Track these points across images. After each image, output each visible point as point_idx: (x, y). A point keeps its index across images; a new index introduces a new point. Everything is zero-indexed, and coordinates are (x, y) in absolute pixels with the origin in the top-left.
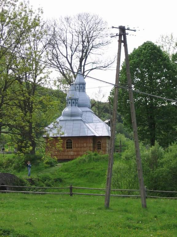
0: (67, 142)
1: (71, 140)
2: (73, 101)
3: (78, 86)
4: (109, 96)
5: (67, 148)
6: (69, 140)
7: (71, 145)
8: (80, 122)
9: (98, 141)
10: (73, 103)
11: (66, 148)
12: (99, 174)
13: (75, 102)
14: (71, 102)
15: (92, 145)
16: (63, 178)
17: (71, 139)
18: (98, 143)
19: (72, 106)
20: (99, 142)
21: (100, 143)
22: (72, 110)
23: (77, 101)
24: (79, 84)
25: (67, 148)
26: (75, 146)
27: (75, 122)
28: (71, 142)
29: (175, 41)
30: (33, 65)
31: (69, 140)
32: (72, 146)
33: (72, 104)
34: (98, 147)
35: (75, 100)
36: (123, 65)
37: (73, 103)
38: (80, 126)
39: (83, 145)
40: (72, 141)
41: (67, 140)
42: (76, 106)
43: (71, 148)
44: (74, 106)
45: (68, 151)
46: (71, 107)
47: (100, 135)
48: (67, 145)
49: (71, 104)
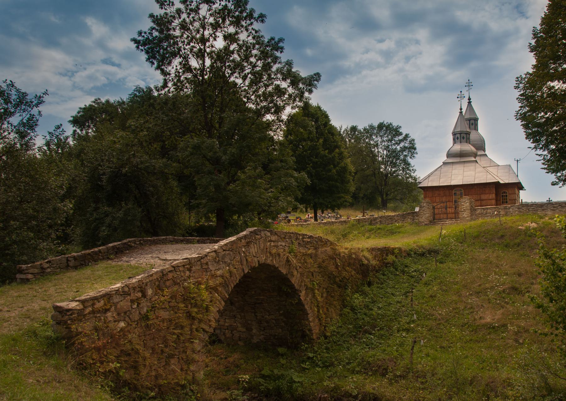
2: (462, 135)
3: (459, 136)
4: (522, 125)
8: (473, 164)
9: (502, 192)
10: (463, 138)
13: (474, 123)
14: (459, 137)
15: (494, 196)
16: (400, 44)
18: (502, 193)
19: (461, 142)
20: (504, 192)
21: (506, 193)
22: (462, 147)
23: (476, 121)
24: (460, 134)
27: (466, 165)
33: (462, 139)
34: (503, 200)
35: (466, 134)
37: (472, 124)
38: (453, 176)
39: (480, 198)
42: (466, 142)
44: (464, 142)
46: (460, 144)
47: (507, 182)
49: (459, 139)
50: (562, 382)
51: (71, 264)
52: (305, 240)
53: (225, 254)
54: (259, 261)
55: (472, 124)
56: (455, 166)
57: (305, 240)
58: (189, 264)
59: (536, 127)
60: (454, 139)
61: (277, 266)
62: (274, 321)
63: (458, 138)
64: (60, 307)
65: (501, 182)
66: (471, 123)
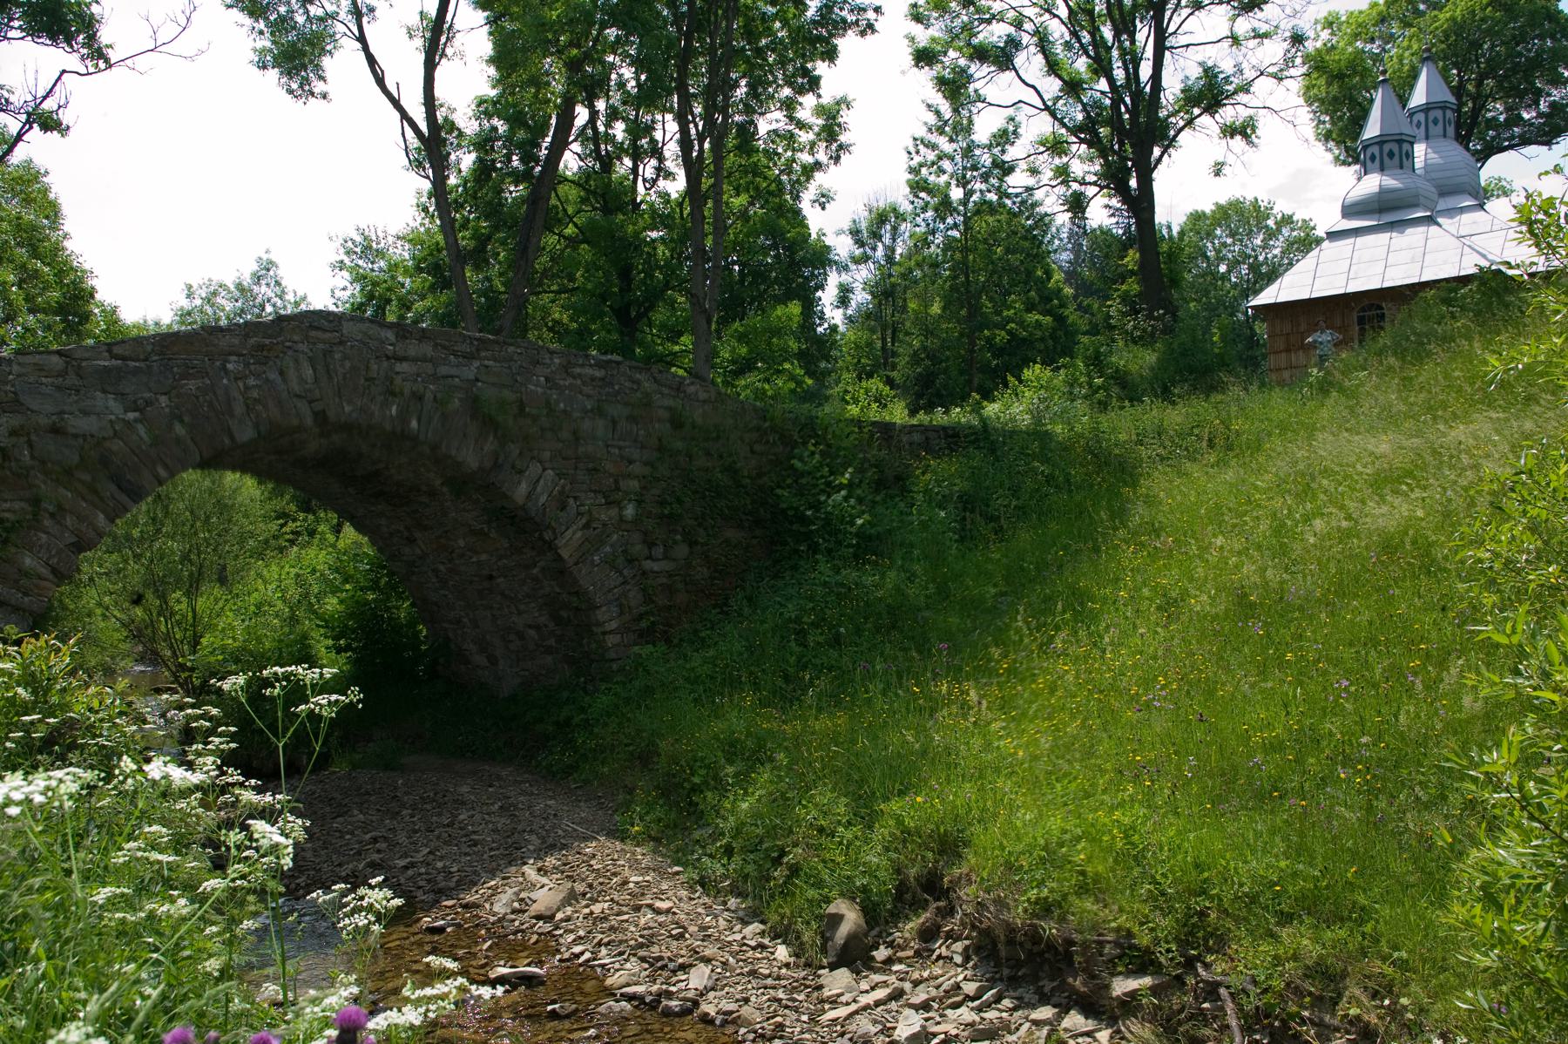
2: (1387, 148)
6: (1370, 307)
23: (1406, 146)
31: (1370, 307)
33: (1386, 159)
41: (1363, 310)
42: (1401, 167)
49: (1397, 158)
56: (1362, 241)
66: (1431, 118)
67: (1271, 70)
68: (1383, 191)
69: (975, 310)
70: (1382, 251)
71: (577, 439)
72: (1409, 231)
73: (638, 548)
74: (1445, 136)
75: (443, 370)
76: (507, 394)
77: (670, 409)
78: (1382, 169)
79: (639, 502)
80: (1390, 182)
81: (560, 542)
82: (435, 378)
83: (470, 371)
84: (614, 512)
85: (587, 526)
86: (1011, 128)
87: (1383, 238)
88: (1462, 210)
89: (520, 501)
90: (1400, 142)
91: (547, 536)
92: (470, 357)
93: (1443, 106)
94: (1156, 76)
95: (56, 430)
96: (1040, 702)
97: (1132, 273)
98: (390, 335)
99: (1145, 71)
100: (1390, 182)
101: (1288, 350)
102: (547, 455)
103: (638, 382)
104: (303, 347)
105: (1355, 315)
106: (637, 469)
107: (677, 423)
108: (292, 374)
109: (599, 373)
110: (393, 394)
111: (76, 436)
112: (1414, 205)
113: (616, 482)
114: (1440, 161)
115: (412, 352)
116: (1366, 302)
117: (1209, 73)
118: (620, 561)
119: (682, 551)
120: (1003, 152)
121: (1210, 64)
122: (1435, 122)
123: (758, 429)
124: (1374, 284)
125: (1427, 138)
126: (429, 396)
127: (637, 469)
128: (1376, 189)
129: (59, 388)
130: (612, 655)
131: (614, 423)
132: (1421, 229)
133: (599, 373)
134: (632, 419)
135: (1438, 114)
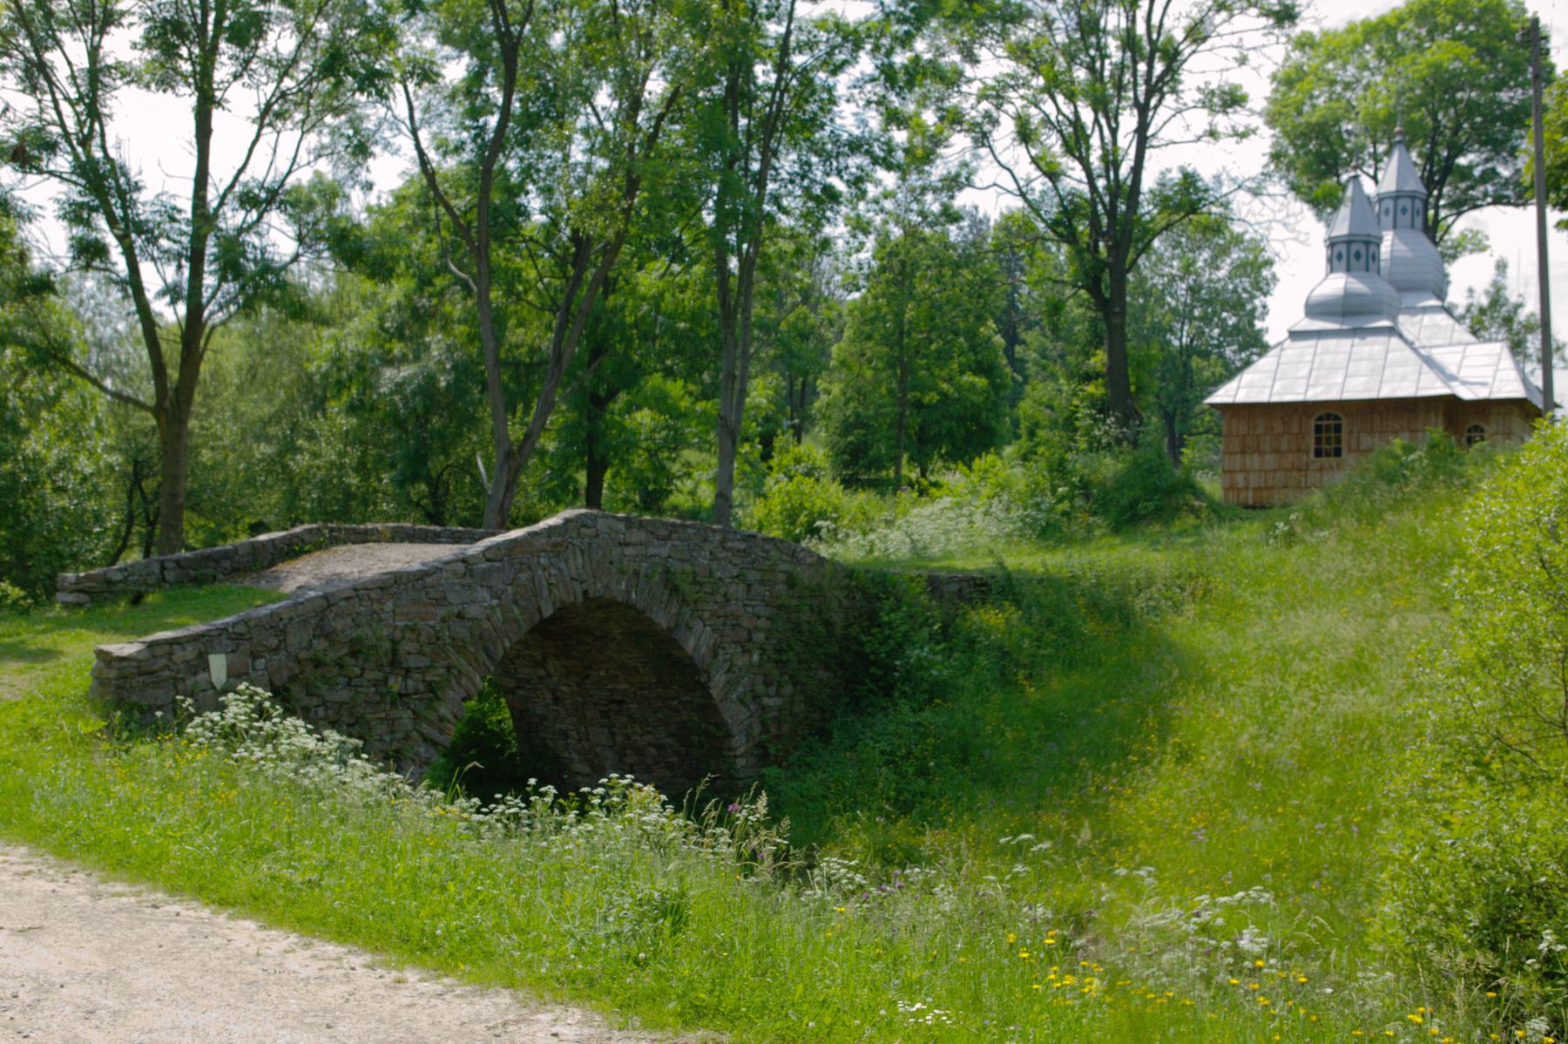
0: (1318, 429)
1: (1337, 418)
2: (1354, 248)
3: (1342, 248)
5: (1318, 453)
6: (1328, 417)
7: (1338, 440)
11: (1312, 453)
12: (1224, 471)
17: (1341, 415)
23: (1372, 248)
25: (1318, 453)
26: (1354, 446)
28: (1338, 428)
29: (1564, 118)
30: (519, 271)
31: (1328, 417)
32: (1344, 446)
33: (1353, 259)
36: (829, 214)
40: (1344, 422)
41: (1320, 419)
42: (1367, 269)
43: (1338, 453)
45: (1321, 469)
48: (1318, 441)
49: (1363, 259)
50: (6, 679)
51: (170, 576)
52: (730, 544)
53: (489, 569)
54: (585, 593)
55: (1387, 212)
56: (1324, 344)
57: (730, 544)
58: (394, 584)
59: (742, 267)
60: (1330, 260)
61: (641, 605)
62: (653, 751)
63: (1358, 256)
64: (107, 653)
65: (1466, 394)
66: (1400, 207)
67: (1248, 184)
68: (1348, 295)
69: (907, 370)
70: (1343, 357)
71: (728, 601)
72: (1370, 339)
73: (760, 688)
74: (1412, 226)
75: (651, 551)
76: (688, 567)
77: (786, 572)
78: (1348, 270)
79: (763, 650)
80: (1358, 286)
81: (712, 684)
82: (647, 557)
83: (664, 552)
84: (746, 659)
85: (729, 671)
86: (964, 173)
87: (1345, 344)
88: (1425, 310)
89: (690, 652)
90: (1367, 243)
91: (703, 679)
92: (668, 538)
93: (1412, 196)
94: (1137, 169)
95: (460, 616)
96: (165, 822)
97: (1098, 375)
98: (621, 526)
99: (1125, 170)
100: (1358, 286)
101: (1243, 452)
102: (707, 614)
103: (767, 551)
104: (577, 542)
105: (1313, 423)
106: (763, 623)
107: (791, 582)
108: (571, 562)
109: (742, 546)
110: (623, 573)
111: (472, 619)
112: (1376, 313)
113: (750, 633)
114: (1410, 254)
115: (634, 539)
116: (1322, 412)
117: (1189, 179)
118: (748, 698)
119: (788, 689)
120: (952, 197)
121: (1190, 170)
122: (1404, 211)
123: (848, 586)
124: (1333, 395)
125: (1395, 227)
126: (642, 572)
127: (763, 623)
128: (1341, 292)
129: (463, 586)
130: (741, 775)
131: (749, 586)
132: (1383, 339)
133: (742, 546)
134: (762, 582)
135: (1406, 203)
